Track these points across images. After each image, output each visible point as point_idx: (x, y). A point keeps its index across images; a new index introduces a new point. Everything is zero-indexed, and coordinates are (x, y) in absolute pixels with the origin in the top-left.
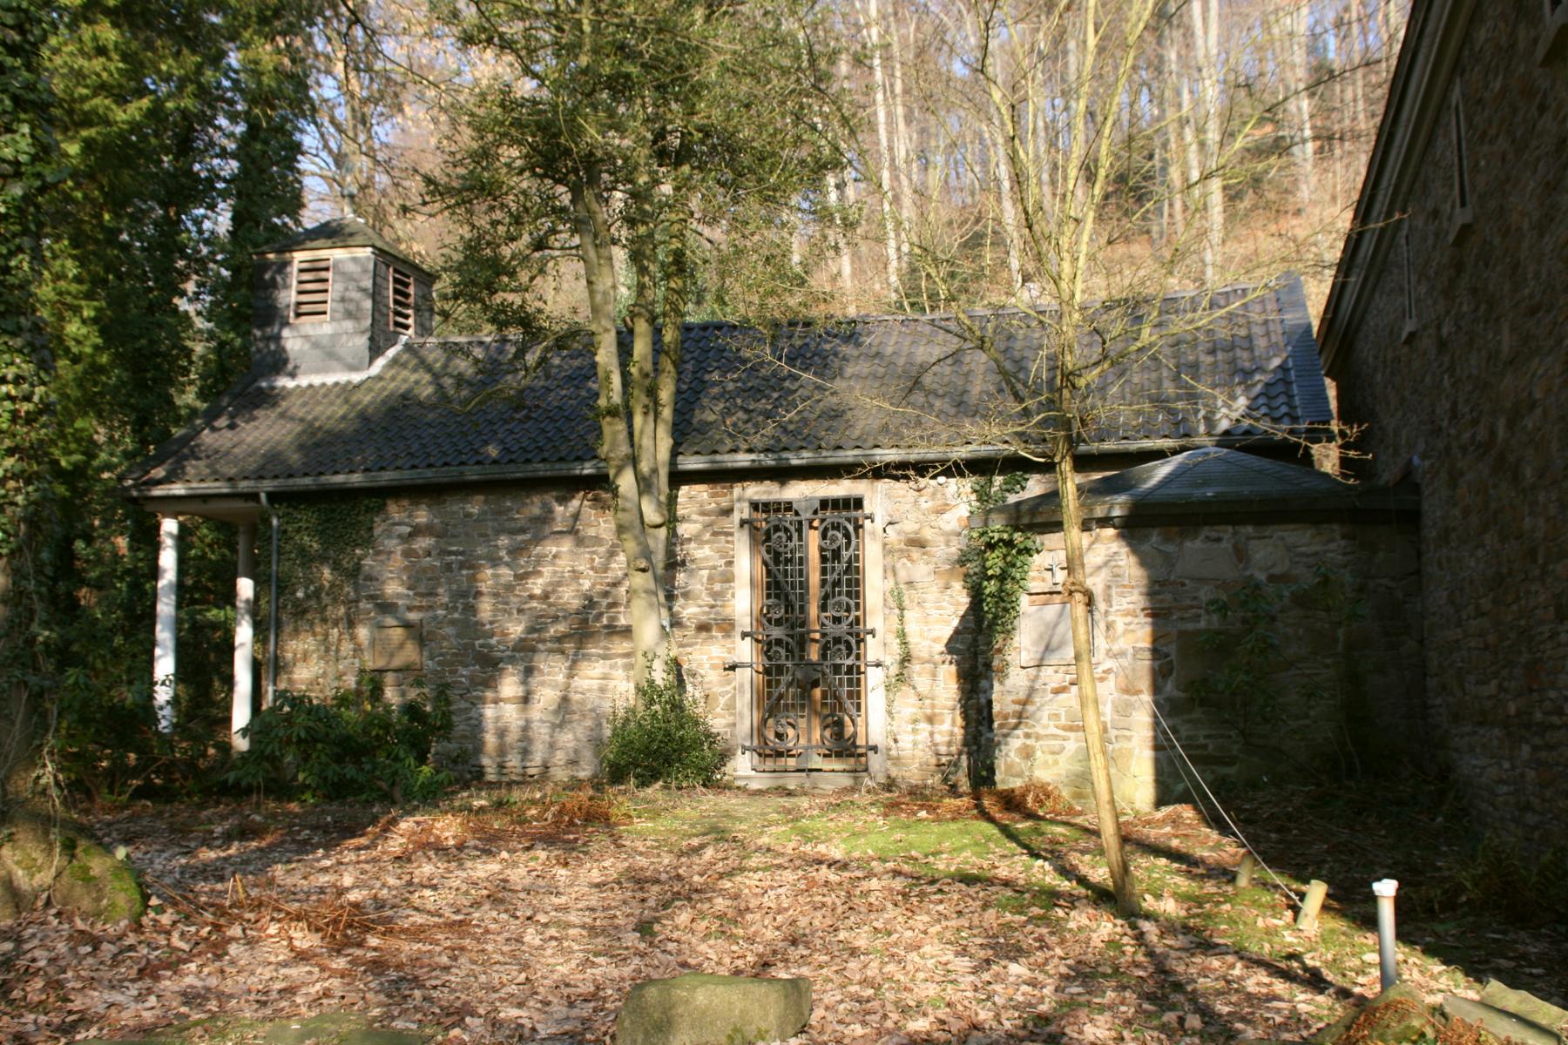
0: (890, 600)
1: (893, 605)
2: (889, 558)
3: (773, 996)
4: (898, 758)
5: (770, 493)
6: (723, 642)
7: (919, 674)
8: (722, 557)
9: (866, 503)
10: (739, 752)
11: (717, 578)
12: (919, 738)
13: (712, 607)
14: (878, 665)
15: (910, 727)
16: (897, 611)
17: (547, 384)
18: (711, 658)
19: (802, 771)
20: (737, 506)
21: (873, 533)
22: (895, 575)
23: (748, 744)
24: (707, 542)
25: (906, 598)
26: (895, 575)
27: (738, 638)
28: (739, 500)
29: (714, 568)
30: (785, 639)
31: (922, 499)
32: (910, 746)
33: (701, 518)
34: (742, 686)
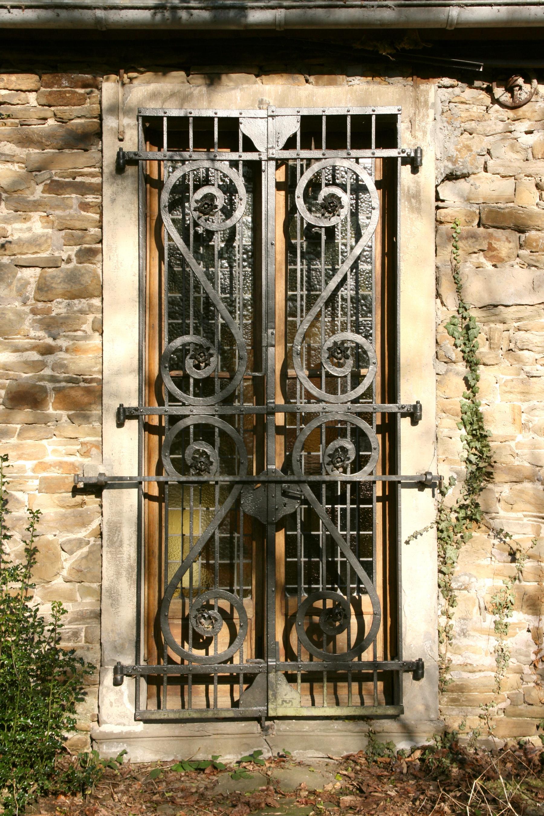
0: (448, 343)
1: (456, 354)
2: (447, 252)
3: (96, 129)
4: (461, 689)
5: (185, 99)
6: (70, 430)
7: (511, 505)
8: (70, 241)
9: (402, 126)
10: (108, 679)
11: (60, 287)
12: (509, 643)
13: (48, 351)
14: (421, 485)
15: (490, 619)
16: (462, 368)
17: (36, 640)
18: (43, 466)
19: (437, 439)
20: (110, 123)
21: (416, 196)
22: (459, 289)
23: (128, 661)
24: (36, 206)
25: (481, 340)
26: (459, 289)
27: (110, 421)
28: (115, 109)
29: (54, 263)
30: (217, 422)
31: (522, 127)
32: (490, 661)
33: (21, 152)
34: (116, 528)
